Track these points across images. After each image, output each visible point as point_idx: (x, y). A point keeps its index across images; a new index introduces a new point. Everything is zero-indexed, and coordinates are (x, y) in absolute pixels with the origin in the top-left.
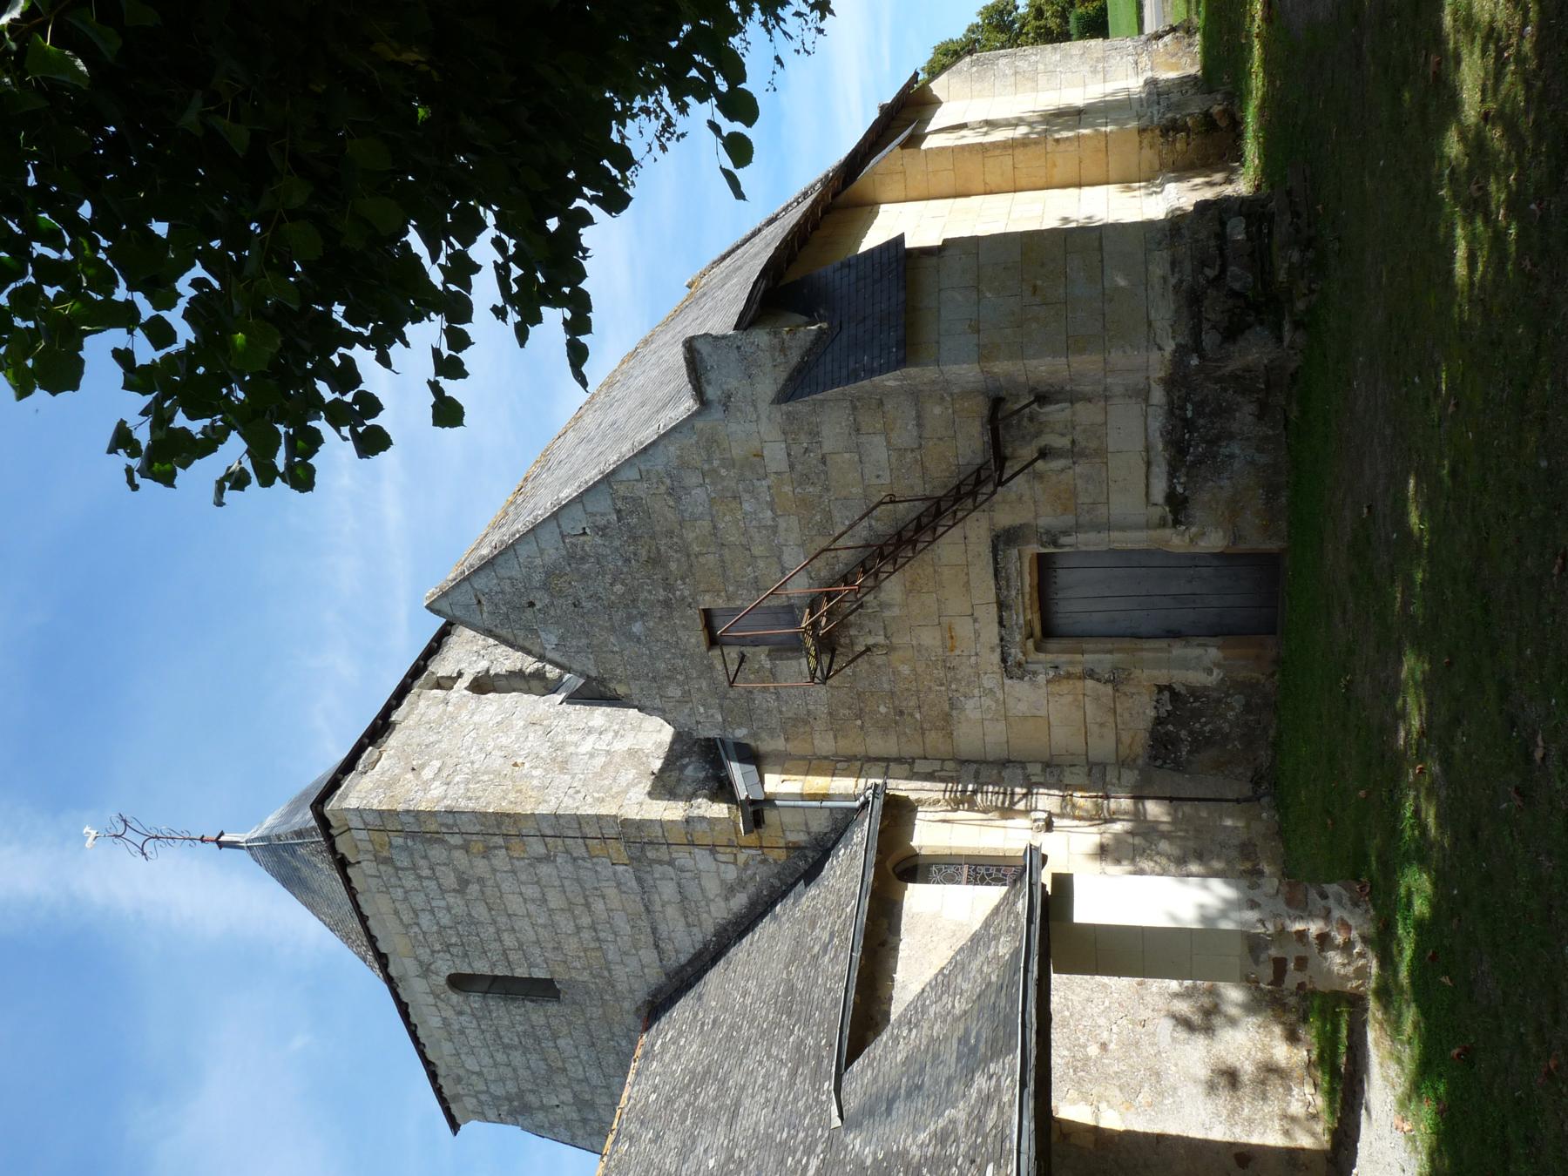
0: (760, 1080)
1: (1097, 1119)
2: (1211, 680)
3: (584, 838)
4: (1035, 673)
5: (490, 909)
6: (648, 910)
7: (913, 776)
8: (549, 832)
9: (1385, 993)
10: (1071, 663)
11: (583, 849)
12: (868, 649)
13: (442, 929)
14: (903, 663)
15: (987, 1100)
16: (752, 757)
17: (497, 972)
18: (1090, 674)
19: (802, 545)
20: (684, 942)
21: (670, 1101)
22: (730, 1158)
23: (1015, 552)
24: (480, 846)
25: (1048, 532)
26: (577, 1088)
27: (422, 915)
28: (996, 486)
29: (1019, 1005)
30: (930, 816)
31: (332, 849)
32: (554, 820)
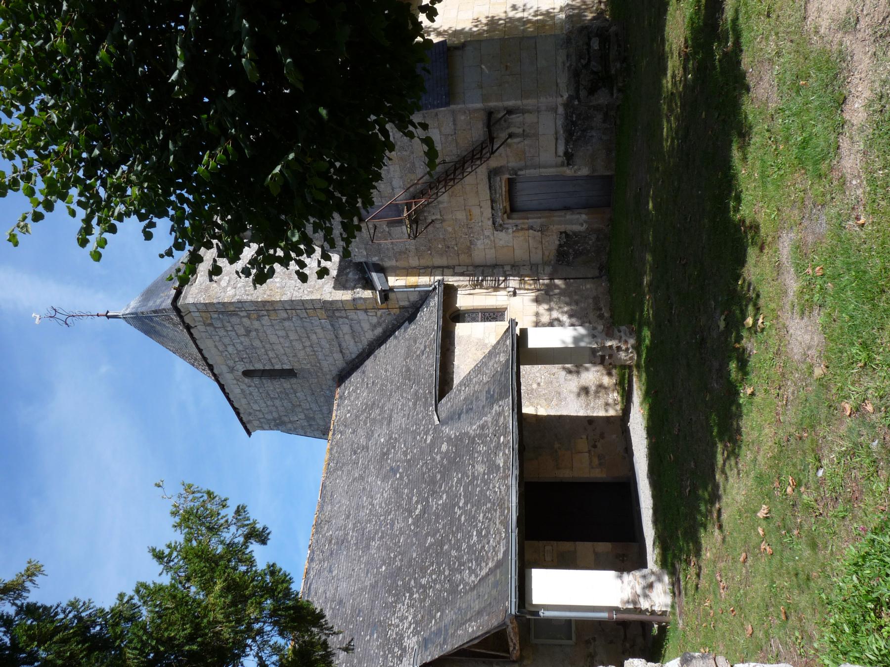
0: (400, 407)
1: (537, 412)
2: (583, 228)
3: (305, 309)
4: (508, 229)
5: (262, 342)
6: (337, 337)
7: (455, 274)
8: (288, 308)
9: (638, 366)
10: (523, 223)
11: (305, 314)
12: (433, 221)
13: (239, 352)
14: (449, 226)
15: (499, 414)
16: (381, 270)
17: (266, 368)
18: (531, 228)
19: (401, 177)
20: (353, 349)
21: (357, 417)
22: (391, 438)
23: (498, 179)
24: (255, 316)
25: (513, 169)
26: (306, 412)
27: (228, 346)
28: (491, 155)
29: (510, 382)
30: (463, 292)
31: (184, 322)
32: (291, 303)
